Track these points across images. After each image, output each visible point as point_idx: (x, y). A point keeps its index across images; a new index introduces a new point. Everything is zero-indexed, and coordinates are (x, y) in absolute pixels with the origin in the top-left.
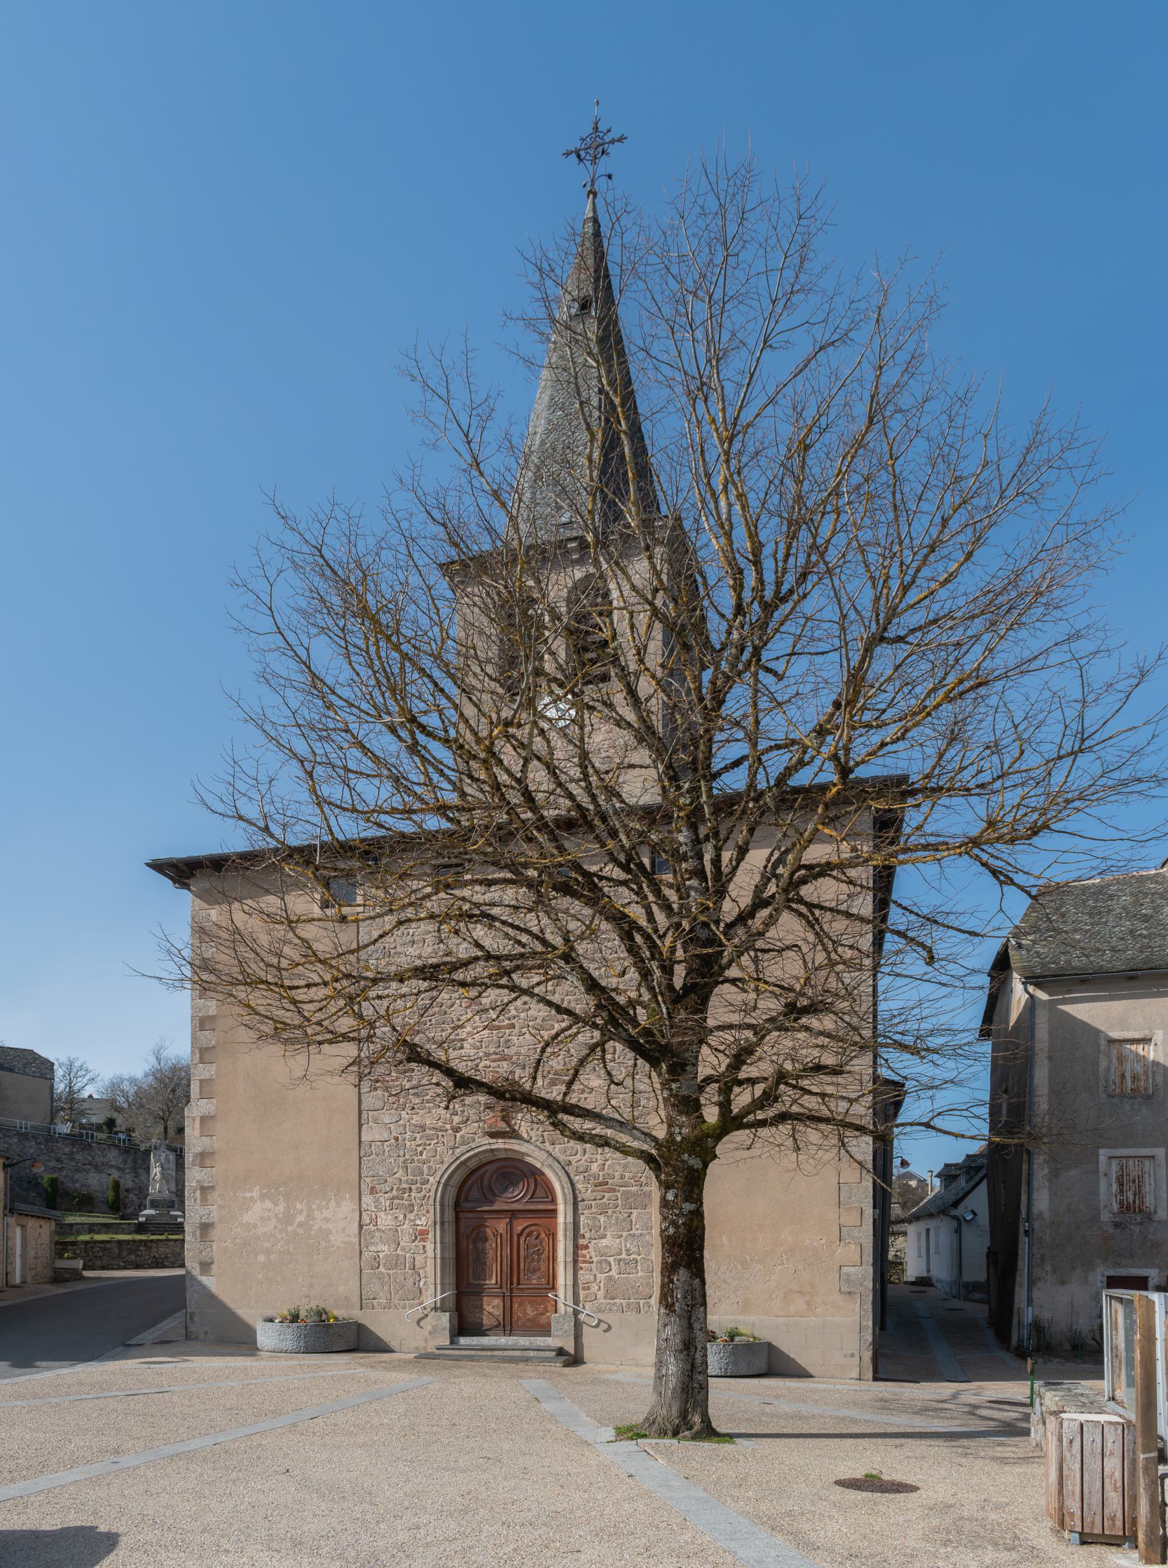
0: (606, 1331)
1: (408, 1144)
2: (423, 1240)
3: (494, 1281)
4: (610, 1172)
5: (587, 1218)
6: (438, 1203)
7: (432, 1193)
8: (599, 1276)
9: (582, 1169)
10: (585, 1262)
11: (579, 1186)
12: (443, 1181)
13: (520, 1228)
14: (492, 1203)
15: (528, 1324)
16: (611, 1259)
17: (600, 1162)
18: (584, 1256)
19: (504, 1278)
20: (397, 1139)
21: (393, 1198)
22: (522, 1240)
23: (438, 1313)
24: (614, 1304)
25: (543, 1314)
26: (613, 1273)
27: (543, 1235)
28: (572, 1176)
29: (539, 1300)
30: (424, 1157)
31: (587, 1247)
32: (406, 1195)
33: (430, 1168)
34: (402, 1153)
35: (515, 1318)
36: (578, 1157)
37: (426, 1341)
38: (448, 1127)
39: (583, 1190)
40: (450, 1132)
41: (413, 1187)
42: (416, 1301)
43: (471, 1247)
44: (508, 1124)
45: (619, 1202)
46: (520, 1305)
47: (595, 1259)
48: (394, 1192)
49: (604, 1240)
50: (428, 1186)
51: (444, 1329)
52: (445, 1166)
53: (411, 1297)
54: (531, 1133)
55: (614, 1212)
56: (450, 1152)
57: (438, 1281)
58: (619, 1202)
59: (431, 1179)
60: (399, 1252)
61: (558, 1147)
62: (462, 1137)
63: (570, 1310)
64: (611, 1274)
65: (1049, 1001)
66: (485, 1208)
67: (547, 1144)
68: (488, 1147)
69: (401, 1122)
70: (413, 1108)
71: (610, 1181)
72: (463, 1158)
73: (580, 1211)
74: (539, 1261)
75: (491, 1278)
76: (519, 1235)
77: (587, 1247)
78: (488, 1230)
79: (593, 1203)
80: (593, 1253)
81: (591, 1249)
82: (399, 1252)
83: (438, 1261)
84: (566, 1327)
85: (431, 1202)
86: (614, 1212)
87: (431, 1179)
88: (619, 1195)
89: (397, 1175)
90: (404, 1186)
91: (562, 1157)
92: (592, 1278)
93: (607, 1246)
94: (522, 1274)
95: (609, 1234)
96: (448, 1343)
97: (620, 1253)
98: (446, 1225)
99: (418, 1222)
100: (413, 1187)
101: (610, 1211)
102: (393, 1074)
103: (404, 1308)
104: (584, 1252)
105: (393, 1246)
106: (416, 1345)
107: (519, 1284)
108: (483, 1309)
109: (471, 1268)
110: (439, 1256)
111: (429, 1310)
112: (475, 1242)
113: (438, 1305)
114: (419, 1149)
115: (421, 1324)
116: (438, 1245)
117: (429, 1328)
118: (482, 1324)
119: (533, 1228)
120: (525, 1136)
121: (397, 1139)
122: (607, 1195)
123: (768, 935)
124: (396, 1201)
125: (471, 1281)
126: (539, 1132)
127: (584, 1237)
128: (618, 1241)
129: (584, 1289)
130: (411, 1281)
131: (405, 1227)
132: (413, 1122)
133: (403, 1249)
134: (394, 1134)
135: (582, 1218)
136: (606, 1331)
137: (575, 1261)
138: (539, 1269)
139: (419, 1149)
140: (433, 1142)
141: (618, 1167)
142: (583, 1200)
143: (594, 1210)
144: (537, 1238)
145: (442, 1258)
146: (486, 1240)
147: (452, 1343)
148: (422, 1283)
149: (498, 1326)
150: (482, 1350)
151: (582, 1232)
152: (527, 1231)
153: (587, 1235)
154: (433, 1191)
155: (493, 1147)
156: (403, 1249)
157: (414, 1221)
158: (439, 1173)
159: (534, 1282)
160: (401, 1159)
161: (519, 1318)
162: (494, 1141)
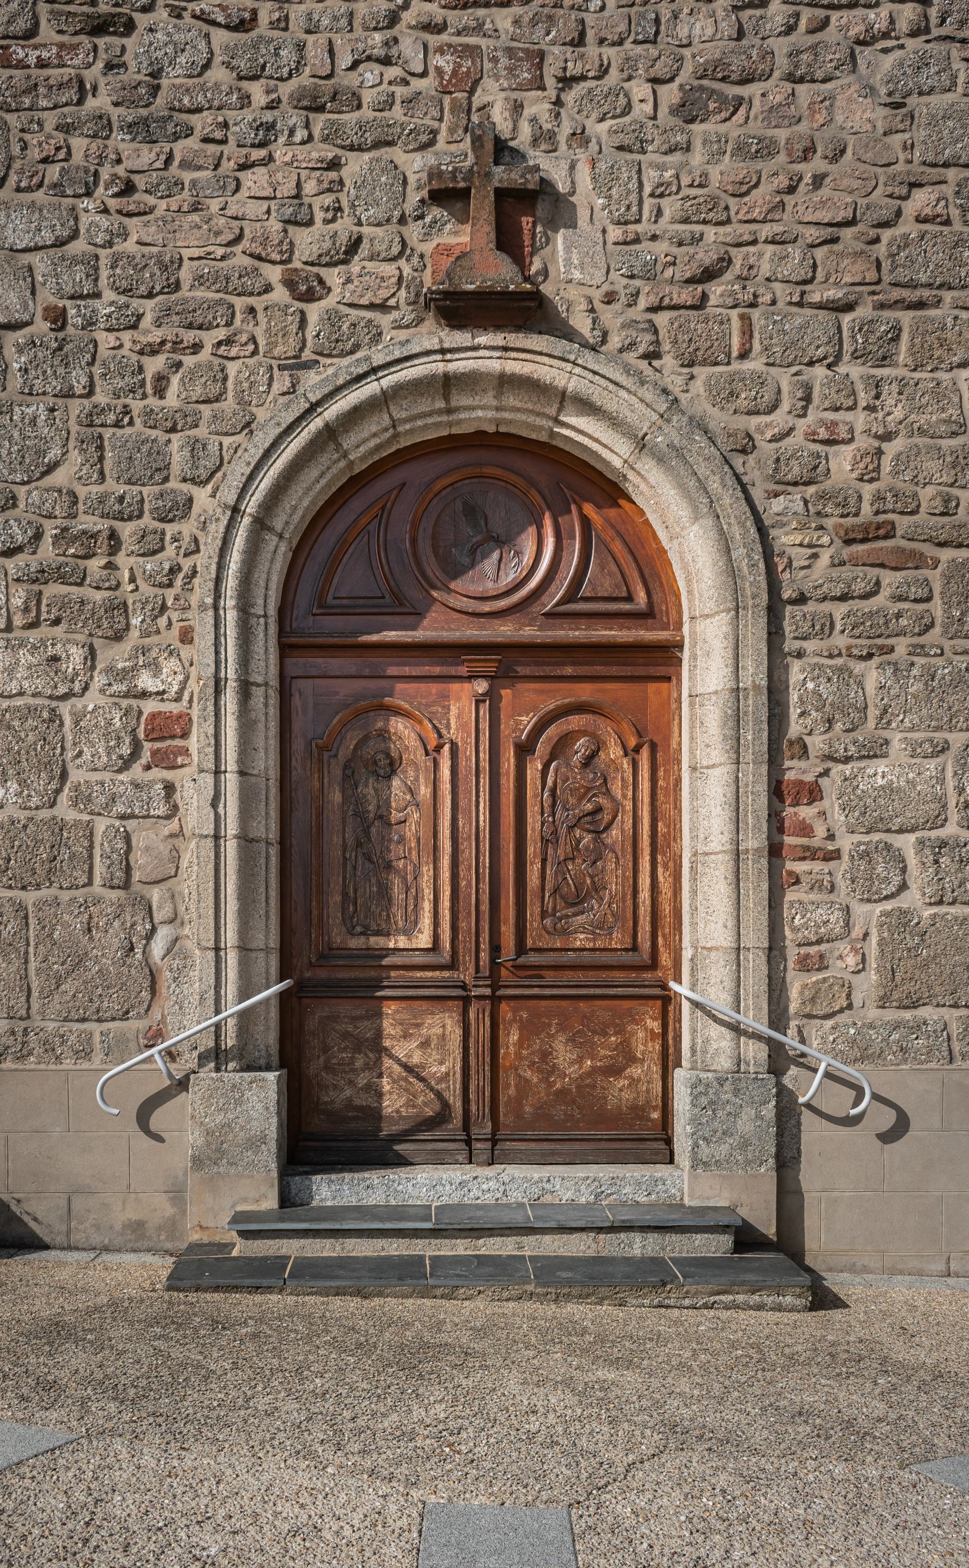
0: (888, 1137)
1: (106, 340)
2: (165, 760)
3: (424, 940)
4: (903, 483)
5: (817, 671)
6: (230, 603)
7: (205, 560)
8: (860, 910)
9: (795, 471)
10: (810, 854)
11: (785, 539)
12: (251, 505)
13: (527, 722)
14: (416, 615)
15: (559, 1112)
16: (907, 843)
17: (863, 442)
18: (805, 830)
19: (467, 924)
20: (58, 318)
21: (41, 576)
22: (534, 768)
23: (232, 1076)
24: (918, 1027)
25: (615, 1071)
26: (913, 899)
27: (614, 751)
28: (757, 494)
29: (602, 1011)
30: (172, 399)
31: (813, 793)
32: (95, 565)
33: (196, 448)
34: (79, 380)
35: (509, 1091)
36: (780, 419)
37: (177, 1194)
38: (274, 274)
39: (800, 556)
40: (280, 294)
41: (127, 530)
42: (134, 1025)
43: (336, 797)
44: (520, 261)
45: (937, 608)
46: (529, 1030)
47: (846, 843)
48: (47, 551)
49: (881, 766)
50: (187, 528)
51: (255, 1143)
52: (263, 439)
53: (112, 1005)
54: (608, 315)
55: (918, 650)
56: (282, 382)
57: (231, 936)
58: (937, 608)
59: (201, 496)
60: (65, 810)
61: (702, 373)
62: (333, 318)
63: (755, 1052)
64: (903, 902)
65: (549, 509)
66: (391, 635)
67: (668, 362)
68: (436, 366)
69: (78, 247)
70: (128, 189)
71: (903, 523)
72: (333, 411)
73: (790, 645)
74: (597, 856)
75: (410, 929)
76: (524, 750)
77: (813, 793)
78: (398, 725)
79: (838, 611)
80: (838, 818)
81: (831, 802)
82: (65, 810)
83: (231, 849)
84: (745, 1125)
85: (202, 591)
86: (918, 650)
87: (201, 496)
88: (936, 578)
89: (59, 478)
90: (88, 522)
91: (718, 419)
92: (836, 916)
93: (889, 789)
94: (533, 911)
95: (896, 740)
96: (271, 1203)
97: (939, 821)
98: (258, 694)
99: (146, 681)
100: (127, 530)
101: (902, 646)
102: (47, 32)
103: (85, 1053)
104: (806, 812)
105: (41, 783)
106: (132, 1214)
107: (521, 949)
108: (377, 1047)
109: (335, 884)
110: (232, 827)
111: (189, 1060)
112: (349, 779)
113: (230, 1040)
114: (153, 365)
115: (157, 1120)
116: (231, 782)
117: (193, 1138)
118: (375, 1115)
119: (575, 722)
120: (581, 323)
121: (58, 318)
122: (889, 578)
123: (141, 326)
124: (53, 590)
125: (338, 936)
126: (638, 312)
127: (804, 752)
128: (931, 765)
129: (805, 965)
130: (114, 939)
131: (91, 701)
132: (130, 246)
133: (81, 798)
134: (47, 297)
135: (796, 672)
136: (888, 1137)
137: (775, 851)
138: (598, 888)
139: (153, 365)
140: (210, 338)
141: (931, 466)
142: (801, 599)
143: (840, 641)
144: (588, 761)
145: (246, 840)
146: (392, 767)
147: (285, 1201)
148: (158, 947)
149: (441, 1118)
150: (435, 1233)
151: (795, 728)
152: (552, 732)
153: (816, 743)
154: (209, 547)
155: (459, 365)
156: (81, 798)
157: (123, 675)
158: (237, 472)
159: (580, 940)
160: (76, 407)
161: (524, 1084)
162: (461, 338)
